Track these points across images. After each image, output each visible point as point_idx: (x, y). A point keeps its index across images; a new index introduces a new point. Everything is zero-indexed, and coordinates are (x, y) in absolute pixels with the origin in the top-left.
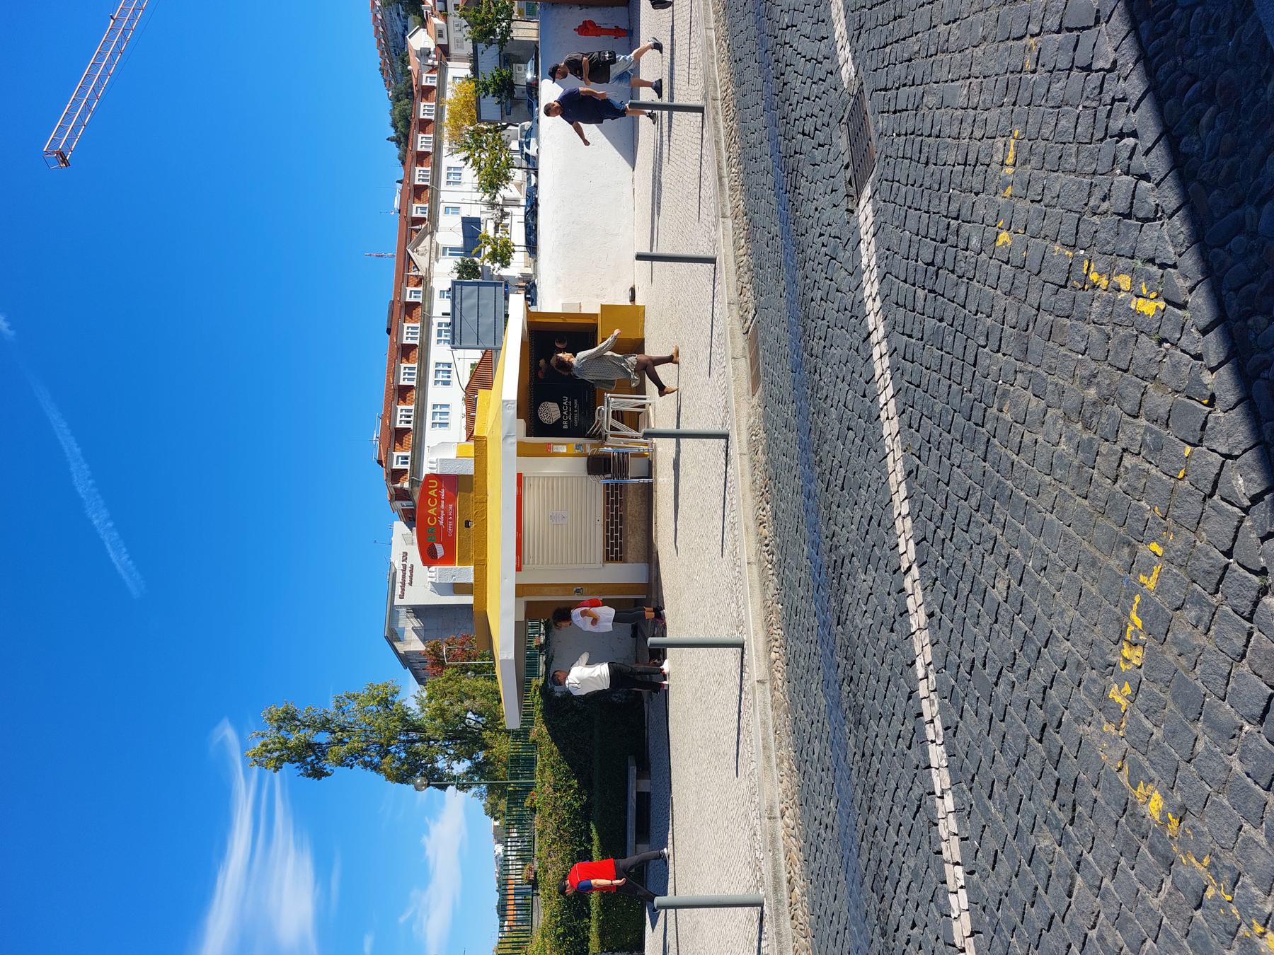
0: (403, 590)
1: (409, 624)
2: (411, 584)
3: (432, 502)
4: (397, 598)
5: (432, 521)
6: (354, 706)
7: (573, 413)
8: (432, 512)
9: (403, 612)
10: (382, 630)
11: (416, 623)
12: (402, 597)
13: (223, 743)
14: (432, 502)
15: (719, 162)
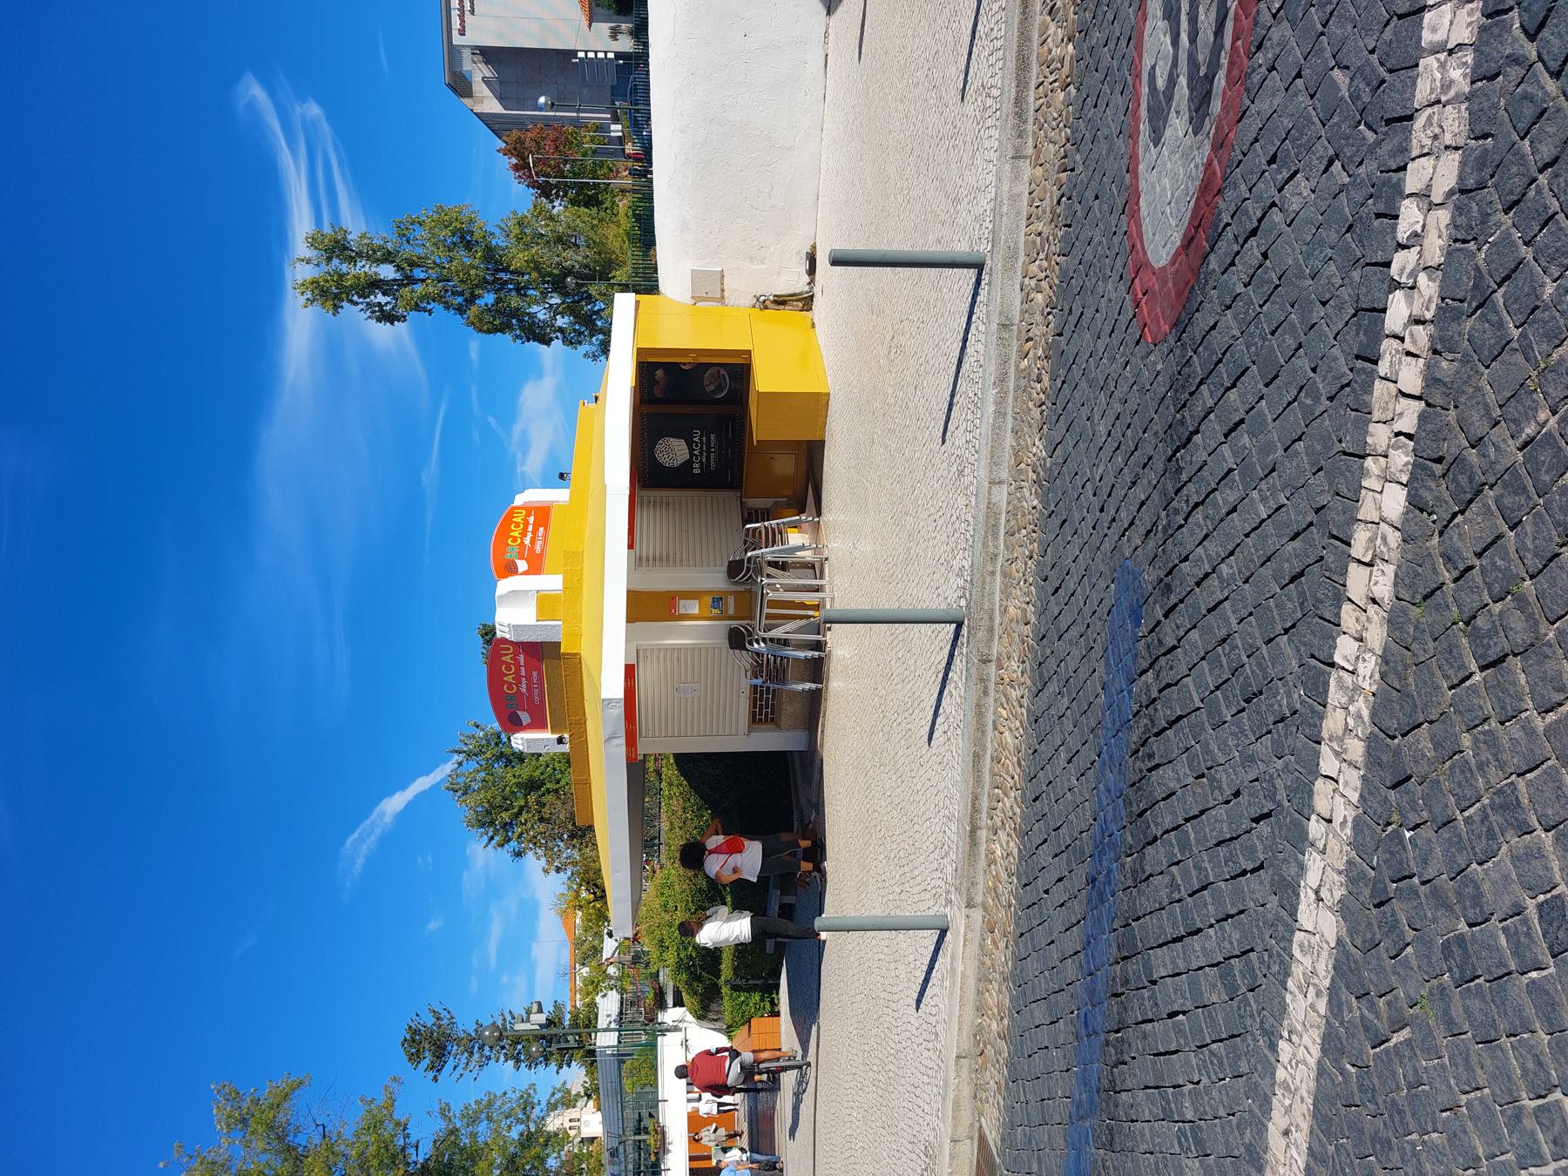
0: (462, 21)
1: (479, 73)
2: (472, 12)
3: (508, 669)
4: (455, 33)
5: (510, 688)
6: (421, 233)
7: (708, 452)
8: (509, 679)
9: (466, 53)
10: (441, 77)
11: (487, 71)
12: (462, 32)
13: (251, 106)
14: (508, 669)
15: (975, 798)
